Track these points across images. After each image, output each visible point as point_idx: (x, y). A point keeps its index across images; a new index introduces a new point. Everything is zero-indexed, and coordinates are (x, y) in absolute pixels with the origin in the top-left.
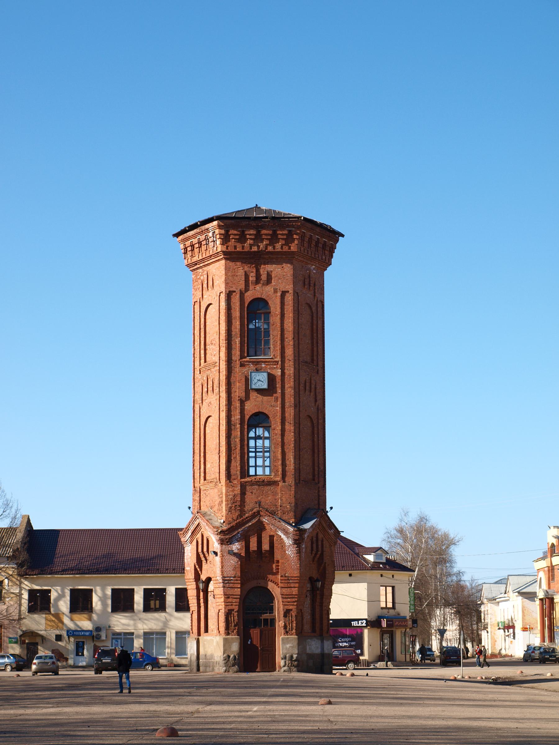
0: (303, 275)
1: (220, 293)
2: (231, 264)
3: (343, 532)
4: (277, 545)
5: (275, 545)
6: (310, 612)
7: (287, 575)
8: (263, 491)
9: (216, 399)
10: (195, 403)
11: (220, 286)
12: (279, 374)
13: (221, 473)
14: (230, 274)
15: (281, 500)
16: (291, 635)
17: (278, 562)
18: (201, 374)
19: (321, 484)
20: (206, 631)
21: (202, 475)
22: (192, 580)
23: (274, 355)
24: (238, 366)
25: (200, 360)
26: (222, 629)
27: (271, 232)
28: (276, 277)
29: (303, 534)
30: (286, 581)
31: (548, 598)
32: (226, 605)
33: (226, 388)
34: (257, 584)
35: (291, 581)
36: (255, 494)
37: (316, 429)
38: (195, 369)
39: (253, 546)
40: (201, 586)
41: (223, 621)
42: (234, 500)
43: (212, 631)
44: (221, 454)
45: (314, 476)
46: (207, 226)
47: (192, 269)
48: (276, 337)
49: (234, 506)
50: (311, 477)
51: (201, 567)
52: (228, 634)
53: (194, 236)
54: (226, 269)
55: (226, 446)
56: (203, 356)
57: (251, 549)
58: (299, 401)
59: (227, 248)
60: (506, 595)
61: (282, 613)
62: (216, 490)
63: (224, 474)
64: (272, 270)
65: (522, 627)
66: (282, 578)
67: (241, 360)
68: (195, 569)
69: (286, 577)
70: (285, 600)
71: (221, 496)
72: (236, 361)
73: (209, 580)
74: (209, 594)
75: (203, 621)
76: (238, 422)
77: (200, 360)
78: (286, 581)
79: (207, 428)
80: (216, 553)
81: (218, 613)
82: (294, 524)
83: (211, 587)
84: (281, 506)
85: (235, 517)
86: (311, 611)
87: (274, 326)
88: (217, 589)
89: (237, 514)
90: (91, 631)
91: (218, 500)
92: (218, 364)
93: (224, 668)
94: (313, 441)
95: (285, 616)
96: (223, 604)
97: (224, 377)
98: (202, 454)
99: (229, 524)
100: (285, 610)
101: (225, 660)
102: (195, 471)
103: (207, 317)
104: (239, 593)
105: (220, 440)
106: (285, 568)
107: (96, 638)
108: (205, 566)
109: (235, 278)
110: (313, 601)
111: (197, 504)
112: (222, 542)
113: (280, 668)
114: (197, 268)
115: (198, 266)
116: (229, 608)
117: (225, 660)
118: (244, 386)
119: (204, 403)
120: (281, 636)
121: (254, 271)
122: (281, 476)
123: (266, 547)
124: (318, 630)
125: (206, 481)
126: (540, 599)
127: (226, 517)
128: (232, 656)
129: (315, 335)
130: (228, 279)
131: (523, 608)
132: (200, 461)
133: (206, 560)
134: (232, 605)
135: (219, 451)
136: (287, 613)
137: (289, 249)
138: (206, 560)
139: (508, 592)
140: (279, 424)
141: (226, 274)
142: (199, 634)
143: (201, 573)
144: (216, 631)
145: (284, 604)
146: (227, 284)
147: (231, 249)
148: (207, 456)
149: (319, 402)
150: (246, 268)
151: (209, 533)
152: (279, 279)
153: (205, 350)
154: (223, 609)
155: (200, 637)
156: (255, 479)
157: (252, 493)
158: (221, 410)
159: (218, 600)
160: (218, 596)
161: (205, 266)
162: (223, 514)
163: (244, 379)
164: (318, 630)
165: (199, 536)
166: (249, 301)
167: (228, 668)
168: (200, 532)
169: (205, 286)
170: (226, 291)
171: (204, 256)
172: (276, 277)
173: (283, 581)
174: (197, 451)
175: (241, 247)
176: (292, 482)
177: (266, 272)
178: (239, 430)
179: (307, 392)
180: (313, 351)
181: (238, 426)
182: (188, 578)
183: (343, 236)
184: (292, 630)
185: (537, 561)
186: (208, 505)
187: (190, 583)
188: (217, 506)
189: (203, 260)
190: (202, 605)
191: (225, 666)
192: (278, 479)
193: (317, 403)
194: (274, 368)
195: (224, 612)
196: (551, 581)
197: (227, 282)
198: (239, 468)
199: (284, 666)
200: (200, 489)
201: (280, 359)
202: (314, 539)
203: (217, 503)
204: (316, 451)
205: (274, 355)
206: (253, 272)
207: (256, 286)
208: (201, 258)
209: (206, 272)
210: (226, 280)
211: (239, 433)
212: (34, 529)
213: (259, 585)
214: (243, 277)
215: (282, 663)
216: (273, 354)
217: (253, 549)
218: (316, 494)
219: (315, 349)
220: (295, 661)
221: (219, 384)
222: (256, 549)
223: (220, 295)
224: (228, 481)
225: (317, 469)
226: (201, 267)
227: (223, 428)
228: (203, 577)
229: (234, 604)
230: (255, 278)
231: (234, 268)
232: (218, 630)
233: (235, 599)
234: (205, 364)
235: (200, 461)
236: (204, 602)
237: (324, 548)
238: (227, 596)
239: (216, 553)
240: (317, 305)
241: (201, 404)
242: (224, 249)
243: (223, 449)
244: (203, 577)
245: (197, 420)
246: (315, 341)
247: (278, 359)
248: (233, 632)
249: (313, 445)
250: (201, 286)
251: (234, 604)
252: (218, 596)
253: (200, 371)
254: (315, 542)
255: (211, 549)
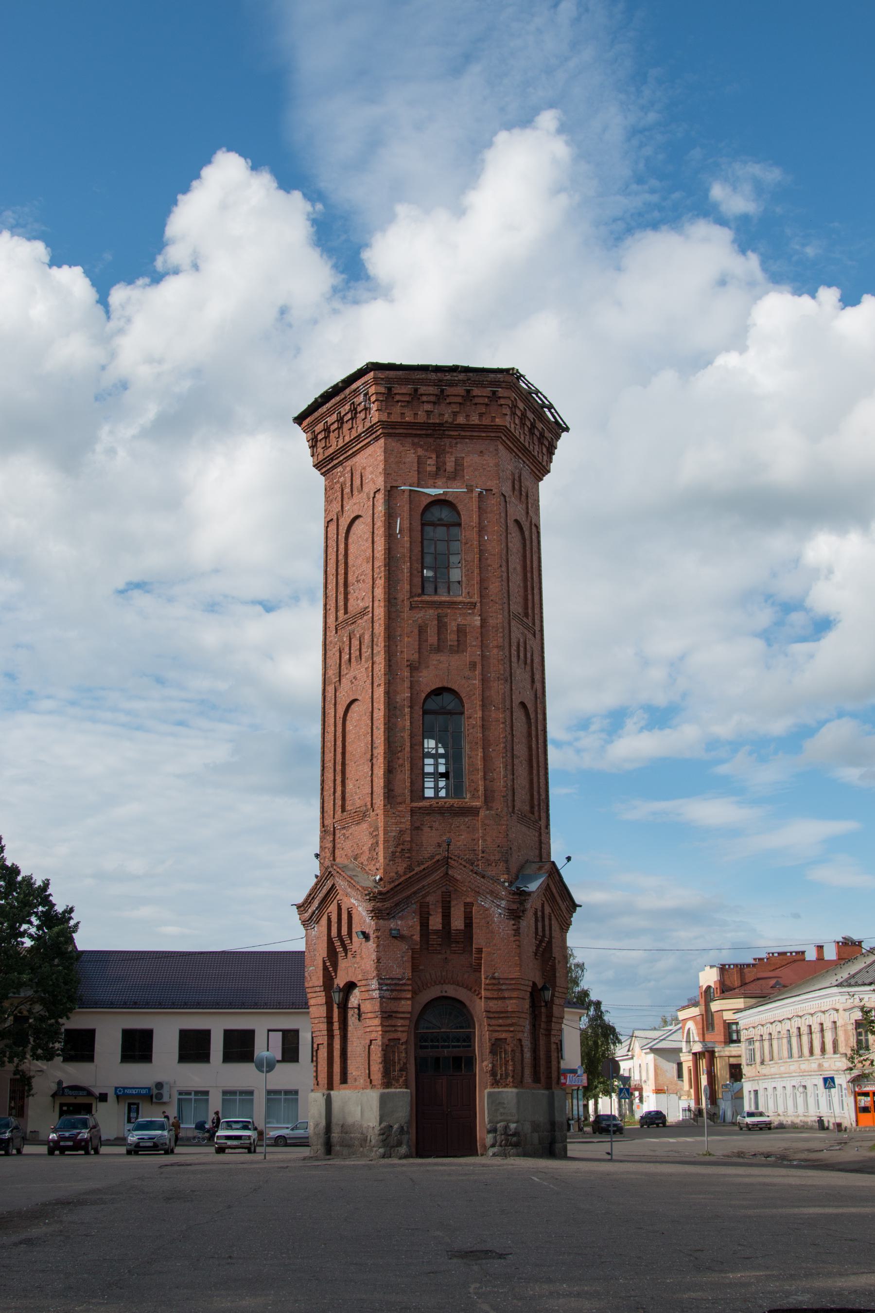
0: (512, 472)
1: (375, 493)
2: (394, 444)
3: (580, 906)
4: (478, 921)
5: (474, 921)
6: (529, 1045)
7: (496, 974)
8: (451, 824)
9: (366, 669)
10: (327, 683)
11: (375, 480)
12: (478, 623)
13: (375, 794)
14: (392, 460)
15: (484, 840)
16: (505, 1087)
17: (480, 951)
18: (339, 633)
19: (543, 823)
20: (344, 1080)
21: (339, 802)
22: (318, 989)
23: (468, 593)
24: (407, 609)
25: (337, 611)
26: (377, 1077)
27: (463, 393)
28: (470, 466)
29: (525, 900)
30: (495, 988)
31: (708, 1051)
32: (384, 1032)
33: (385, 646)
34: (442, 992)
35: (504, 987)
36: (437, 830)
37: (533, 728)
38: (328, 629)
39: (436, 922)
40: (337, 997)
41: (380, 1060)
42: (399, 839)
43: (356, 1080)
44: (375, 760)
45: (532, 807)
46: (354, 386)
47: (324, 470)
48: (471, 564)
49: (399, 850)
50: (527, 808)
51: (335, 965)
52: (387, 1084)
53: (329, 413)
54: (385, 452)
55: (385, 745)
56: (341, 603)
57: (430, 928)
58: (511, 672)
59: (388, 417)
60: (630, 1053)
61: (487, 1046)
62: (364, 826)
63: (382, 794)
64: (463, 455)
65: (654, 1089)
66: (488, 981)
67: (411, 600)
68: (325, 968)
69: (494, 978)
70: (493, 1022)
71: (374, 834)
72: (403, 601)
73: (351, 986)
74: (350, 1013)
75: (339, 1063)
76: (407, 703)
77: (337, 611)
78: (495, 988)
79: (348, 723)
80: (366, 936)
81: (369, 1046)
82: (507, 884)
83: (354, 1000)
84: (483, 852)
85: (401, 870)
86: (531, 1043)
87: (468, 545)
88: (367, 1002)
89: (405, 865)
90: (149, 1089)
91: (367, 841)
92: (370, 609)
93: (382, 1150)
94: (530, 748)
95: (493, 1052)
96: (379, 1028)
97: (382, 628)
98: (339, 768)
99: (390, 883)
100: (493, 1040)
101: (383, 1134)
102: (326, 798)
103: (350, 540)
104: (409, 1009)
105: (374, 738)
106: (493, 963)
107: (156, 1098)
108: (342, 964)
109: (402, 466)
110: (534, 1027)
111: (328, 855)
112: (378, 914)
113: (485, 1148)
114: (335, 467)
115: (335, 462)
116: (391, 1037)
117: (383, 1134)
118: (417, 643)
119: (344, 680)
120: (485, 1089)
121: (434, 456)
122: (482, 799)
123: (458, 923)
124: (543, 1079)
125: (345, 813)
126: (693, 1053)
127: (385, 870)
128: (396, 1126)
129: (529, 575)
130: (390, 467)
131: (656, 1068)
132: (335, 780)
133: (346, 950)
134: (396, 1031)
135: (372, 755)
136: (496, 1046)
137: (492, 422)
138: (346, 950)
139: (632, 1049)
140: (478, 708)
141: (386, 461)
142: (330, 1086)
143: (336, 975)
144: (361, 1081)
145: (491, 1028)
146: (387, 474)
147: (396, 418)
148: (348, 769)
149: (538, 685)
150: (420, 452)
151: (353, 901)
152: (476, 470)
153: (346, 594)
154: (380, 1038)
155: (332, 1093)
156: (438, 803)
157: (431, 827)
158: (375, 685)
159: (369, 1022)
160: (369, 1015)
161: (347, 458)
162: (378, 865)
163: (416, 631)
164: (543, 1079)
165: (333, 908)
166: (425, 504)
167: (388, 1148)
168: (335, 901)
169: (347, 490)
170: (385, 487)
171: (347, 439)
172: (470, 466)
173: (490, 987)
174: (329, 765)
175: (413, 416)
176: (372, 948)
177: (454, 459)
178: (407, 717)
179: (521, 662)
180: (526, 600)
181: (407, 710)
182: (310, 985)
183: (567, 429)
184: (506, 1078)
185: (684, 1008)
186: (350, 854)
187: (314, 995)
188: (368, 852)
189: (346, 447)
190: (337, 1032)
191: (384, 1146)
192: (477, 804)
193: (535, 686)
194: (469, 613)
195: (380, 1043)
196: (705, 1032)
197: (387, 472)
198: (408, 784)
199: (493, 1146)
200: (334, 828)
201: (479, 600)
202: (539, 914)
203: (366, 848)
204: (535, 765)
205: (468, 593)
206: (431, 458)
207: (436, 481)
208: (341, 444)
209: (348, 469)
210: (385, 469)
211: (408, 723)
212: (79, 949)
213: (444, 994)
214: (416, 465)
215: (489, 1139)
216: (467, 591)
217: (435, 928)
218: (537, 839)
219: (530, 597)
220: (513, 1135)
221: (373, 641)
222: (440, 927)
223: (374, 497)
224: (389, 806)
225: (537, 797)
226: (340, 463)
227: (380, 715)
228: (340, 981)
229: (400, 1029)
230: (435, 467)
231: (400, 450)
232: (369, 1077)
233: (402, 1021)
234: (346, 616)
235: (335, 780)
236: (340, 1028)
237: (553, 932)
238: (387, 1016)
239: (366, 936)
240: (531, 529)
241: (338, 684)
242: (384, 418)
243: (380, 750)
244: (340, 981)
245: (331, 712)
246: (529, 584)
247: (476, 599)
248: (398, 1081)
249: (530, 756)
250: (339, 494)
251: (400, 1029)
252: (369, 1015)
253: (336, 629)
254: (540, 919)
255: (356, 928)
